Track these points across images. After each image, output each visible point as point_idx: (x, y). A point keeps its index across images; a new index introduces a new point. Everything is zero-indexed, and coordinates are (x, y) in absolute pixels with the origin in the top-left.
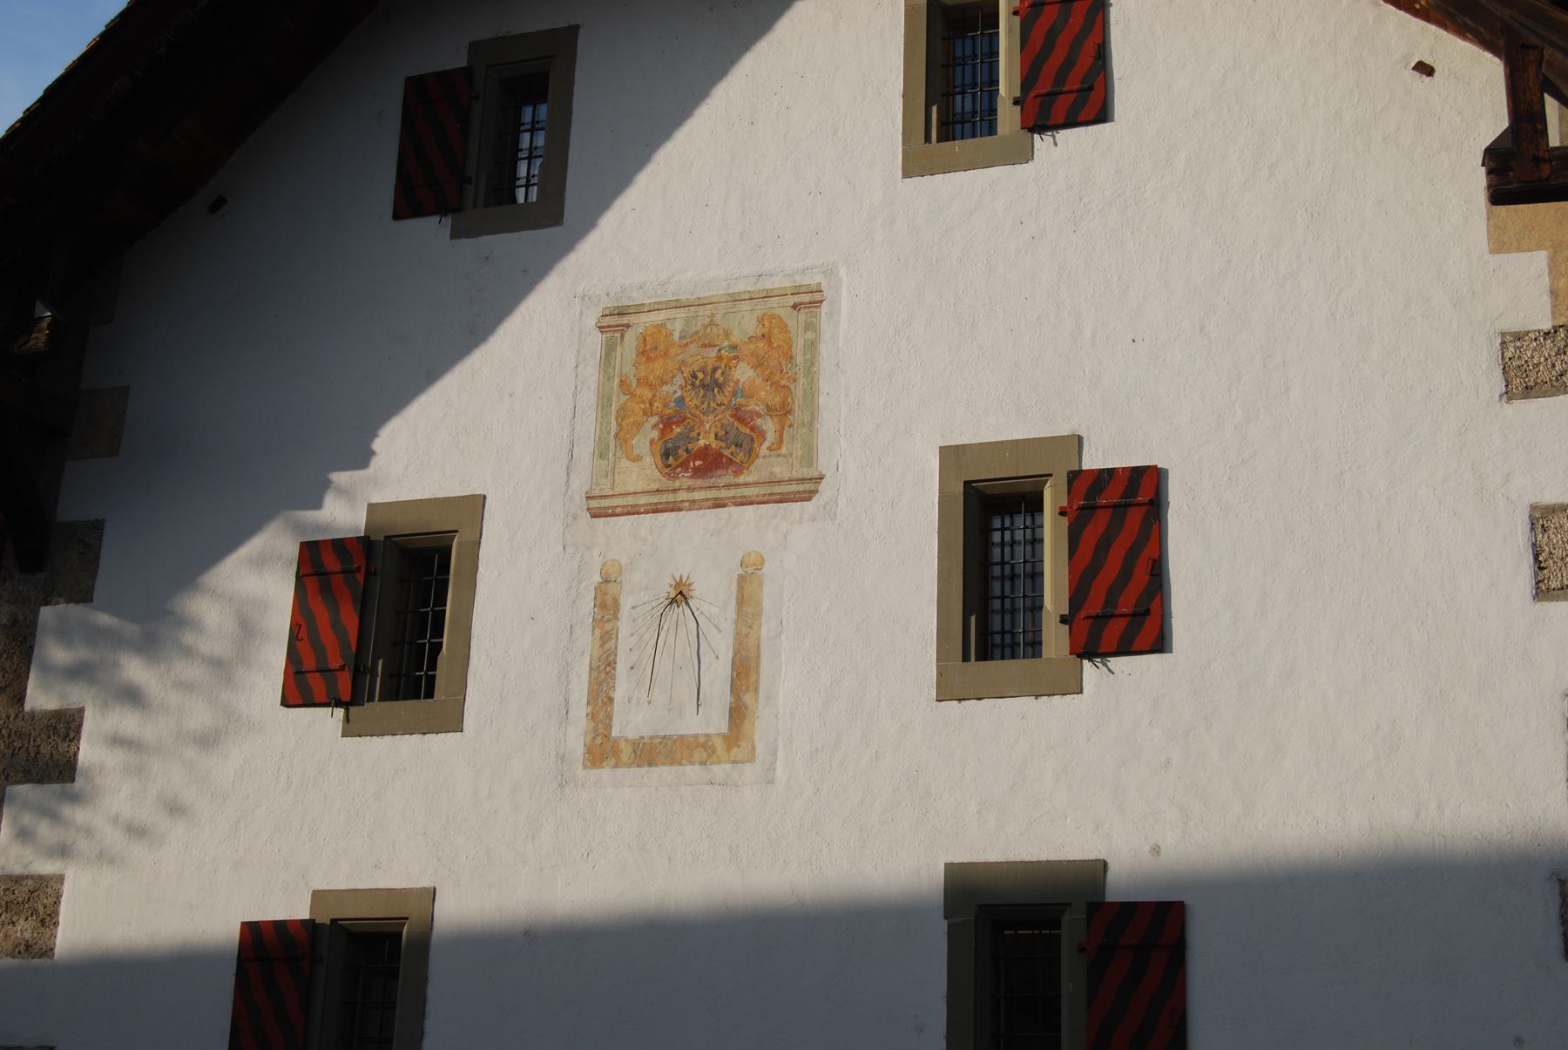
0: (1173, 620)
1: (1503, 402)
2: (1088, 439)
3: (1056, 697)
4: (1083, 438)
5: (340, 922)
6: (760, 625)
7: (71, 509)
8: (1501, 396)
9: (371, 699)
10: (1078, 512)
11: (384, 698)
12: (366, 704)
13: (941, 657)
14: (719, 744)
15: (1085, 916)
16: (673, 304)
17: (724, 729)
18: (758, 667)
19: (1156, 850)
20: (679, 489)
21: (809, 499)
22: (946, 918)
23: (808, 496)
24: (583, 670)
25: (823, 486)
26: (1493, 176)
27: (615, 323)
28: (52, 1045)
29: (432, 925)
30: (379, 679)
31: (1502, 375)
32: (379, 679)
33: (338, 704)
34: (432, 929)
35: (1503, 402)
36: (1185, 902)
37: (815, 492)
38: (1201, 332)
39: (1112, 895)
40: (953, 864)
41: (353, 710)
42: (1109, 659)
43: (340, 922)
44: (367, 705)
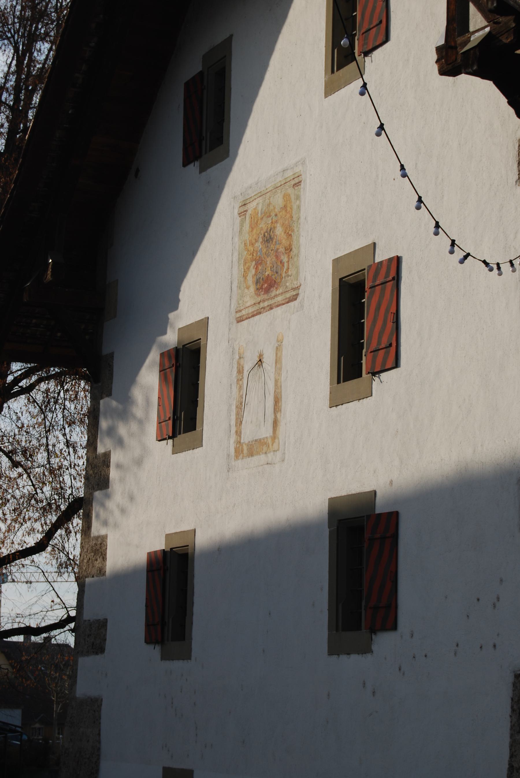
0: (401, 347)
1: (517, 185)
2: (378, 244)
3: (365, 399)
4: (376, 244)
5: (173, 550)
6: (281, 374)
7: (106, 351)
8: (516, 182)
9: (180, 434)
10: (370, 290)
11: (185, 432)
12: (178, 436)
13: (331, 384)
14: (270, 441)
15: (336, 528)
16: (259, 195)
17: (272, 434)
18: (281, 400)
19: (391, 482)
20: (260, 302)
21: (296, 299)
22: (329, 528)
23: (294, 298)
24: (234, 407)
25: (300, 291)
26: (437, 63)
27: (242, 211)
28: (101, 617)
29: (195, 548)
30: (182, 422)
31: (517, 167)
32: (182, 422)
33: (170, 438)
34: (195, 550)
35: (517, 185)
36: (399, 511)
37: (297, 295)
38: (415, 168)
39: (377, 511)
40: (332, 498)
41: (175, 439)
42: (380, 374)
43: (173, 550)
44: (179, 436)
